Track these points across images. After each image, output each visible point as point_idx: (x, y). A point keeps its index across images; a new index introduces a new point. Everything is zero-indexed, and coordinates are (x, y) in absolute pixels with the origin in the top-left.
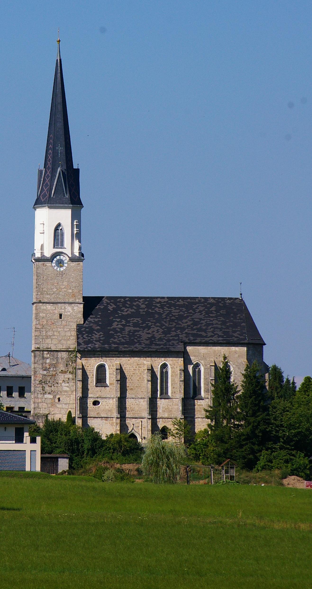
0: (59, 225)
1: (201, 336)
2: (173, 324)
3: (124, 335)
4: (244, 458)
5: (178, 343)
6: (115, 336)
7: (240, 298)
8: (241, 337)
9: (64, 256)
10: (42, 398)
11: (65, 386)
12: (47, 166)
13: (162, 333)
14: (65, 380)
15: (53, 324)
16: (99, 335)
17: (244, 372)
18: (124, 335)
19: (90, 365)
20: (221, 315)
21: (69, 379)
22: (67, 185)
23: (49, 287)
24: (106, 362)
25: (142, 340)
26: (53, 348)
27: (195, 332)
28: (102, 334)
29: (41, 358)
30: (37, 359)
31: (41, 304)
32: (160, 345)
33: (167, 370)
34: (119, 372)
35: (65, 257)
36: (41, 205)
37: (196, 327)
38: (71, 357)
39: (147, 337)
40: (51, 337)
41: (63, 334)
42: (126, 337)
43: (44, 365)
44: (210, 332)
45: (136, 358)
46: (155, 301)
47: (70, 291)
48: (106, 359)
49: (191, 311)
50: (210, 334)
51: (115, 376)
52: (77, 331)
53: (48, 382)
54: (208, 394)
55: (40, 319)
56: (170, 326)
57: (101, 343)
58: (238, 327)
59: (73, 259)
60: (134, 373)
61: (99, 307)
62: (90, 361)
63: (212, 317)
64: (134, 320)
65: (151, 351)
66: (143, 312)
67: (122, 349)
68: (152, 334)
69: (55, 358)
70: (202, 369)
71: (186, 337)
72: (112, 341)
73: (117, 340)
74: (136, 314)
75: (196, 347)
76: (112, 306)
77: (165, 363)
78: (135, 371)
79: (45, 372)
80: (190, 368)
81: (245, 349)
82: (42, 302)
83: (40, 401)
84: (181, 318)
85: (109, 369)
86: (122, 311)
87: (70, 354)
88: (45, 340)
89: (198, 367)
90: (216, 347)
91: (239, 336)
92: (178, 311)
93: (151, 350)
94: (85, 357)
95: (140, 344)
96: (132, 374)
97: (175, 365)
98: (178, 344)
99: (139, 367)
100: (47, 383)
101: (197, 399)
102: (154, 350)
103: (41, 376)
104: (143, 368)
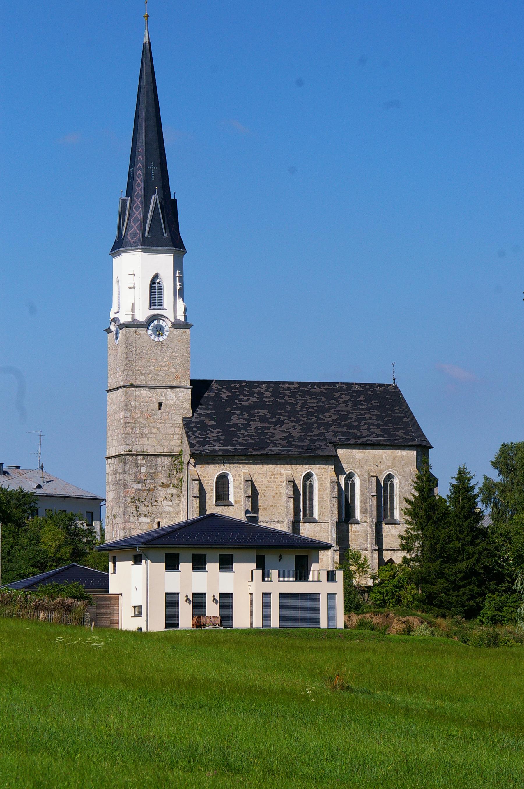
0: (156, 276)
1: (355, 435)
2: (313, 418)
3: (251, 432)
4: (463, 606)
5: (325, 445)
6: (238, 435)
7: (394, 385)
8: (407, 437)
9: (164, 321)
10: (136, 523)
11: (168, 506)
12: (135, 194)
13: (300, 431)
14: (167, 496)
15: (150, 416)
16: (216, 433)
17: (455, 482)
18: (251, 432)
19: (208, 474)
20: (374, 407)
21: (172, 496)
22: (165, 219)
23: (144, 364)
24: (229, 470)
25: (276, 440)
26: (151, 452)
27: (344, 429)
28: (220, 432)
29: (133, 465)
30: (128, 466)
31: (133, 389)
32: (302, 447)
33: (312, 483)
34: (250, 484)
35: (166, 322)
36: (130, 248)
37: (345, 423)
38: (176, 465)
39: (283, 436)
40: (147, 435)
41: (163, 431)
42: (253, 435)
43: (138, 474)
44: (364, 430)
45: (270, 465)
46: (281, 387)
47: (173, 370)
48: (230, 467)
49: (332, 401)
50: (365, 433)
51: (242, 491)
52: (185, 428)
53: (143, 500)
54: (366, 517)
55: (132, 410)
56: (308, 421)
57: (222, 444)
58: (390, 425)
59: (176, 325)
60: (268, 486)
61: (208, 394)
62: (207, 469)
63: (362, 409)
64: (260, 412)
65: (292, 456)
66: (269, 401)
67: (252, 452)
68: (288, 432)
69: (153, 466)
70: (358, 481)
71: (335, 436)
72: (235, 441)
73: (243, 440)
74: (260, 405)
75: (349, 450)
76: (225, 393)
77: (309, 472)
78: (269, 484)
79: (139, 486)
80: (342, 478)
81: (415, 453)
82: (135, 386)
83: (132, 526)
84: (321, 410)
85: (234, 480)
86: (241, 400)
87: (173, 460)
88: (139, 440)
89: (351, 478)
90: (376, 451)
91: (405, 436)
92: (315, 401)
93: (292, 453)
94: (201, 464)
95: (275, 445)
96: (265, 488)
97: (323, 475)
98: (327, 446)
99: (275, 478)
100: (143, 502)
101: (351, 524)
102: (296, 453)
103: (134, 491)
104: (279, 480)
